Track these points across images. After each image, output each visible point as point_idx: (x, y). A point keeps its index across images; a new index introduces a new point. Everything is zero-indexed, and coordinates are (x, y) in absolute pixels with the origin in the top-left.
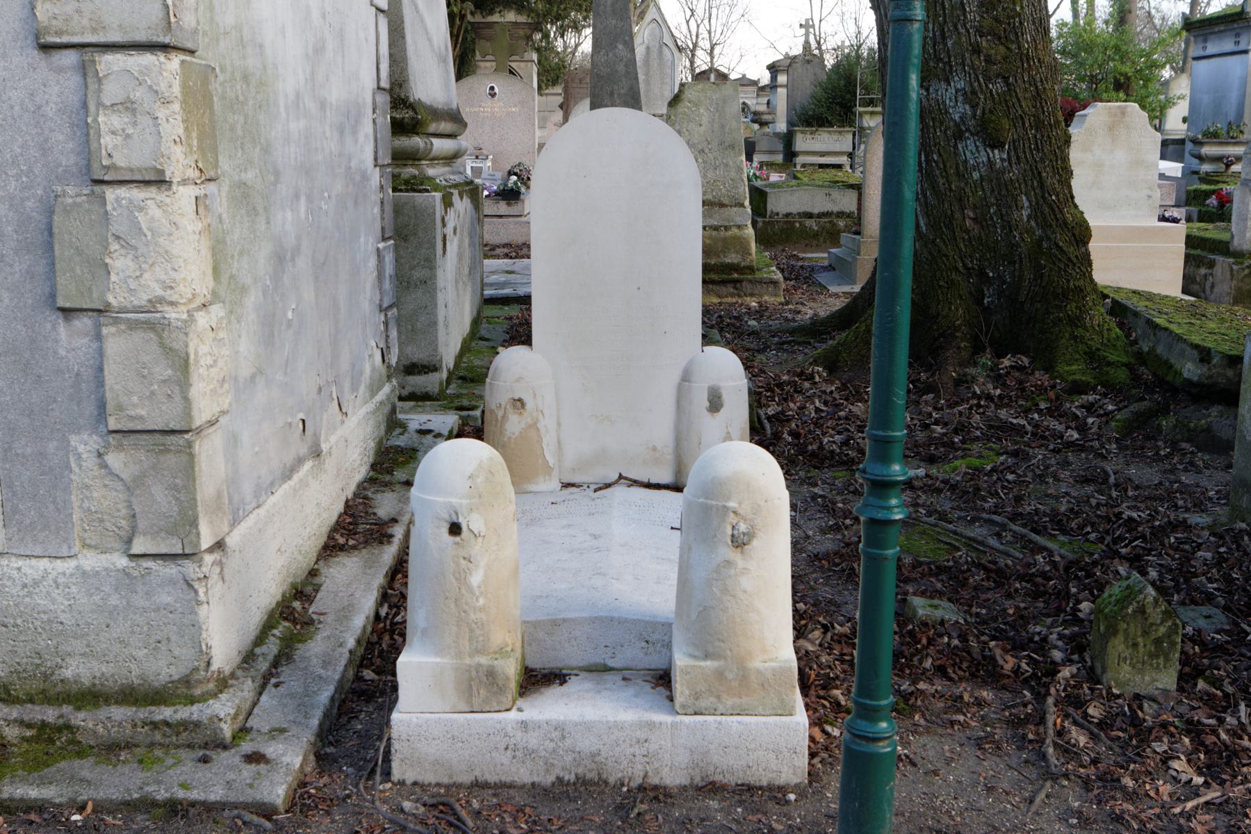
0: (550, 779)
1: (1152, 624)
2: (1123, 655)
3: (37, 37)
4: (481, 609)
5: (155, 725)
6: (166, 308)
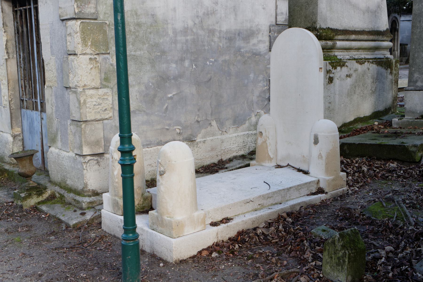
1: (337, 250)
2: (327, 261)
3: (60, 16)
4: (117, 183)
5: (75, 200)
6: (78, 88)
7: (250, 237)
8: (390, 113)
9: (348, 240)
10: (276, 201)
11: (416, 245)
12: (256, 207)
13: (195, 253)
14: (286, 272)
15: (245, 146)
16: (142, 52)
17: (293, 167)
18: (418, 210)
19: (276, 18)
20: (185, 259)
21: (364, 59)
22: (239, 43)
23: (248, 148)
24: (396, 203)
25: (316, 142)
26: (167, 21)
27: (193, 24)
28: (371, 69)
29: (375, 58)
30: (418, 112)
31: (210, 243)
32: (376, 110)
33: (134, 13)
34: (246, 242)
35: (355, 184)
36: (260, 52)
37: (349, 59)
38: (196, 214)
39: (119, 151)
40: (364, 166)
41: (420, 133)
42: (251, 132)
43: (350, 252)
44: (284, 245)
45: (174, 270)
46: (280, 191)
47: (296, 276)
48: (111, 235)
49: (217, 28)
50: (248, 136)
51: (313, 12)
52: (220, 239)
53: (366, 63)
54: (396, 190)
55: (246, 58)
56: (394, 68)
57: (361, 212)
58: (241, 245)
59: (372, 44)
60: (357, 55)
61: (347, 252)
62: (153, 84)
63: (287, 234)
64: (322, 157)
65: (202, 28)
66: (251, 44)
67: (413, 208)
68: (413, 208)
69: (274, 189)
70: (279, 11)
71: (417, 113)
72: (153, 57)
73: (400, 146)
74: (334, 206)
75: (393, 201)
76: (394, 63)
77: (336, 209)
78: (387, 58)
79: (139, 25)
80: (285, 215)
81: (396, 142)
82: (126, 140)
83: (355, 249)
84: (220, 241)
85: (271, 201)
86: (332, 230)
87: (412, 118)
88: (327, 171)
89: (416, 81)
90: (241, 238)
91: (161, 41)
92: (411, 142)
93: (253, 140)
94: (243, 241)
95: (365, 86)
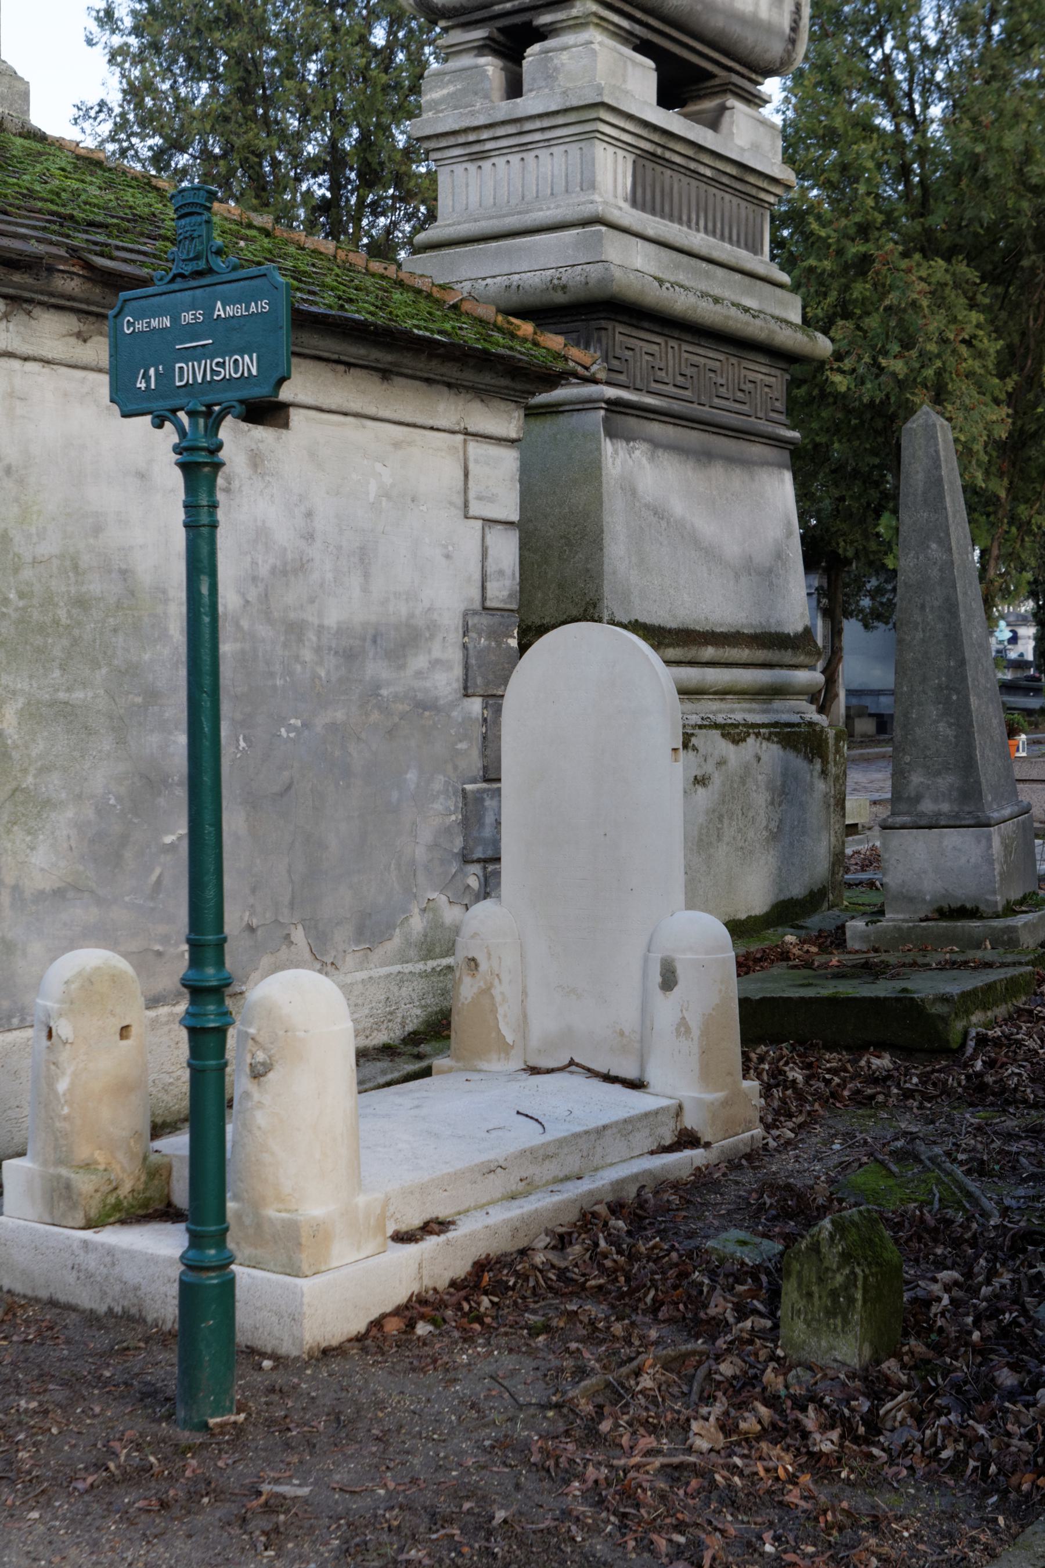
0: (102, 1309)
1: (827, 1269)
4: (66, 1118)
7: (517, 1274)
8: (825, 905)
9: (856, 1237)
10: (566, 1171)
11: (1022, 1264)
12: (514, 1188)
13: (359, 1326)
14: (673, 1354)
15: (391, 1013)
16: (90, 694)
17: (589, 1070)
18: (996, 1179)
19: (483, 588)
20: (335, 1343)
21: (744, 725)
22: (375, 668)
23: (399, 1020)
24: (928, 1162)
25: (669, 981)
26: (164, 592)
27: (242, 602)
28: (765, 758)
29: (776, 724)
30: (928, 898)
31: (400, 1297)
32: (782, 898)
33: (68, 563)
34: (508, 1288)
35: (782, 1119)
36: (437, 699)
37: (701, 727)
38: (361, 1200)
39: (185, 986)
40: (792, 1069)
41: (946, 961)
42: (408, 968)
43: (867, 1271)
44: (631, 1292)
45: (313, 1377)
46: (577, 1136)
47: (700, 1363)
48: (37, 1300)
49: (310, 619)
50: (402, 981)
51: (588, 570)
52: (428, 1282)
53: (751, 740)
54: (911, 1133)
55: (396, 719)
56: (831, 757)
57: (832, 1194)
58: (496, 1299)
59: (764, 677)
60: (720, 711)
61: (857, 1270)
62: (119, 799)
63: (609, 1276)
64: (688, 1030)
65: (267, 617)
66: (410, 672)
67: (980, 1176)
68: (980, 1176)
69: (557, 1131)
70: (491, 567)
71: (924, 900)
72: (122, 711)
73: (898, 1000)
74: (737, 1183)
75: (918, 1159)
76: (831, 742)
77: (750, 1192)
78: (811, 724)
79: (81, 603)
80: (602, 1209)
81: (882, 989)
82: (210, 954)
83: (878, 1264)
84: (427, 1292)
85: (551, 1169)
86: (765, 1242)
87: (907, 917)
88: (707, 1075)
89: (918, 799)
90: (486, 1276)
91: (147, 657)
92: (926, 986)
93: (414, 996)
94: (499, 1288)
95: (750, 814)
